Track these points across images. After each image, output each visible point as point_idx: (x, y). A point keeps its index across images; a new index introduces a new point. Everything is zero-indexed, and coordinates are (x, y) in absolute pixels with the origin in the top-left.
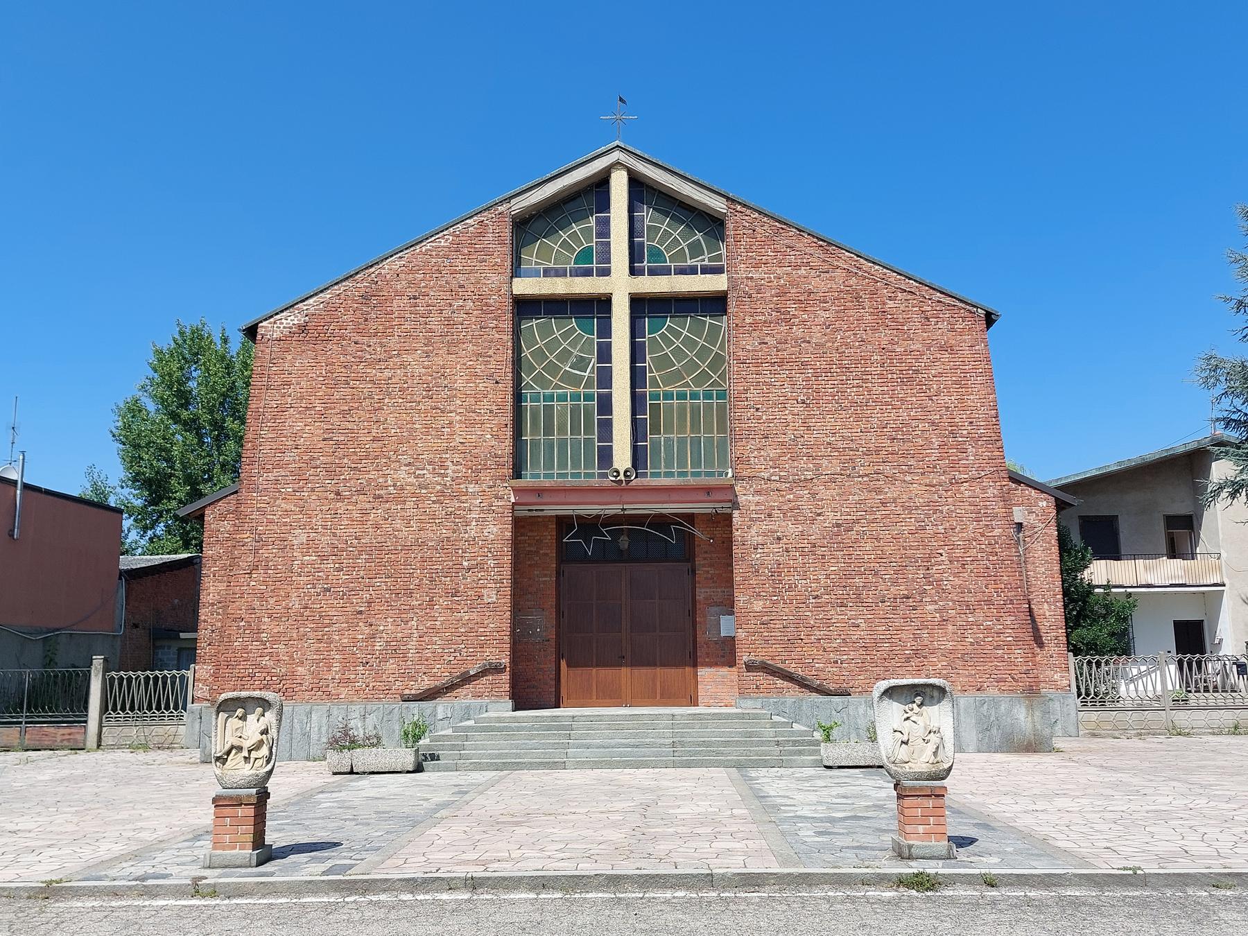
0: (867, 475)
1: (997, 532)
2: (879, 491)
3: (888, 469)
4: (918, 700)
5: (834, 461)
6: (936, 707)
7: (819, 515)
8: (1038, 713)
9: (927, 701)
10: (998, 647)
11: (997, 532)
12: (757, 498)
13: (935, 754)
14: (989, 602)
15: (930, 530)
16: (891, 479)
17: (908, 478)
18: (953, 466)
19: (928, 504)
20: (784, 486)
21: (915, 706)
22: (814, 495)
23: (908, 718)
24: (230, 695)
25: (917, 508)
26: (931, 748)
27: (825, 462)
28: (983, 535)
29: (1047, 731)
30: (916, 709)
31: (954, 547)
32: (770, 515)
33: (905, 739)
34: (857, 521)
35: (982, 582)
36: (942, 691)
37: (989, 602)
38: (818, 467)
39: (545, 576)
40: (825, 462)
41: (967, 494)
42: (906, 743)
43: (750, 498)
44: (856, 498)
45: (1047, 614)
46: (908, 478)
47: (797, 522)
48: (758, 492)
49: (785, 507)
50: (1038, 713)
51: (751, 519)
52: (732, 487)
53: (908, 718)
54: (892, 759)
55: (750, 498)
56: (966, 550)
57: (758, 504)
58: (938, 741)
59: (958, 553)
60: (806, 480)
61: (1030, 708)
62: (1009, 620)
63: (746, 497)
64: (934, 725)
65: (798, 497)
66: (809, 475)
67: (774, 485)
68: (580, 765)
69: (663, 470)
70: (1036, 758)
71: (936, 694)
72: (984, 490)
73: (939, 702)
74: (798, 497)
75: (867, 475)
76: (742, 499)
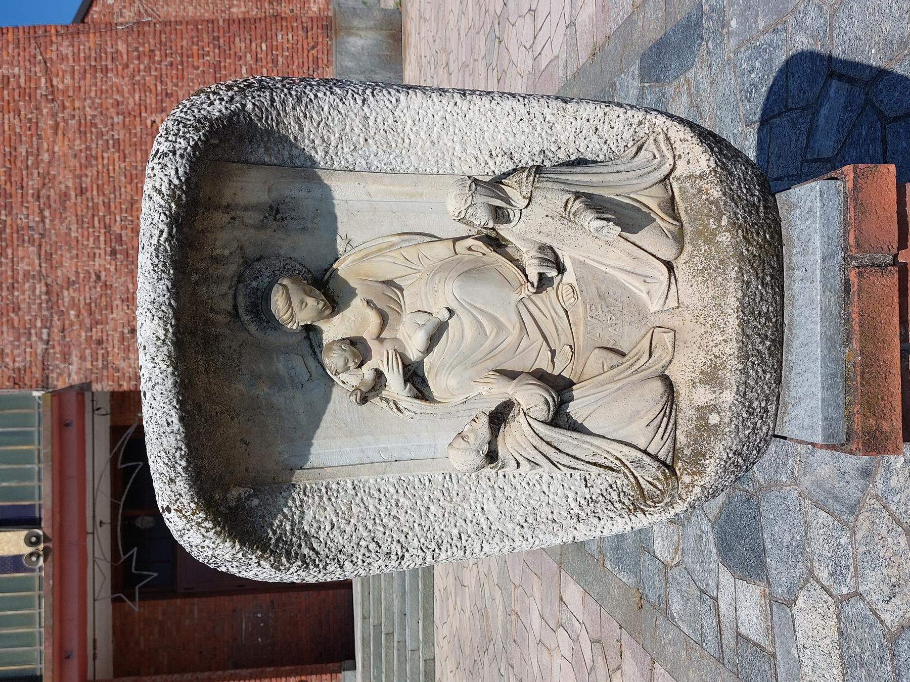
0: (41, 211)
1: (122, 47)
2: (65, 196)
3: (33, 183)
4: (292, 307)
5: (21, 253)
6: (344, 192)
7: (98, 277)
8: (355, 22)
9: (301, 246)
10: (275, 62)
11: (122, 47)
12: (75, 359)
13: (627, 218)
14: (217, 67)
15: (119, 134)
16: (47, 179)
17: (46, 157)
18: (28, 94)
19: (82, 133)
20: (57, 323)
21: (333, 330)
22: (69, 283)
23: (414, 377)
24: (159, 179)
25: (88, 148)
26: (592, 246)
27: (22, 267)
28: (126, 66)
29: (377, 14)
30: (354, 319)
31: (142, 106)
32: (100, 342)
33: (532, 400)
34: (108, 228)
35: (191, 74)
36: (228, 148)
37: (217, 67)
38: (27, 275)
39: (191, 611)
40: (22, 267)
41: (68, 80)
42: (560, 388)
43: (74, 368)
44: (74, 227)
45: (243, 9)
46: (46, 157)
47: (110, 307)
48: (66, 357)
49: (87, 321)
50: (355, 22)
51: (105, 367)
52: (58, 396)
53: (414, 377)
54: (649, 473)
55: (74, 368)
56: (145, 89)
57: (82, 358)
58: (551, 199)
59: (151, 100)
60: (47, 293)
61: (349, 31)
62: (240, 45)
63: (71, 374)
64: (452, 210)
65: (73, 304)
66: (40, 288)
67: (57, 337)
68: (429, 640)
69: (35, 483)
70: (411, 27)
71: (251, 187)
72: (63, 58)
73: (305, 169)
74: (73, 304)
75: (41, 211)
76: (75, 379)
